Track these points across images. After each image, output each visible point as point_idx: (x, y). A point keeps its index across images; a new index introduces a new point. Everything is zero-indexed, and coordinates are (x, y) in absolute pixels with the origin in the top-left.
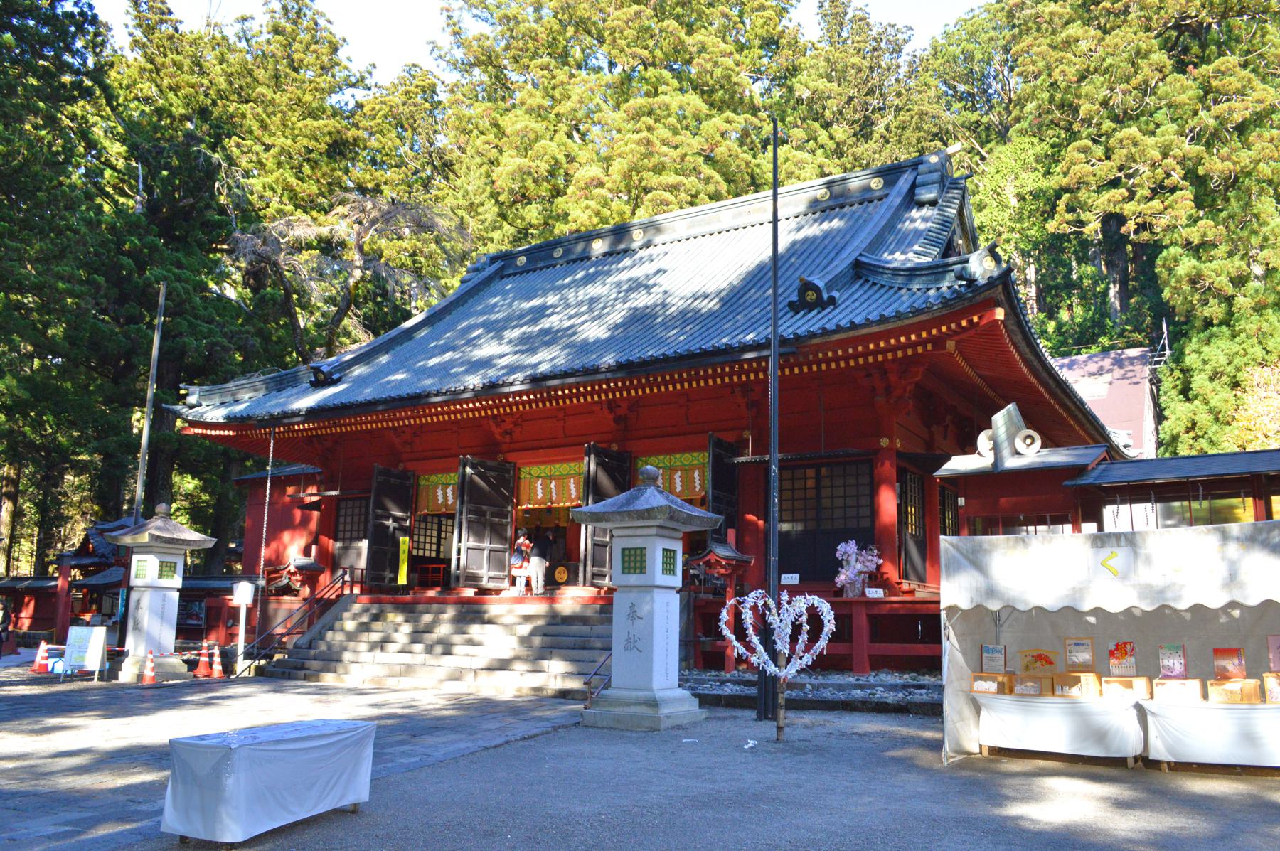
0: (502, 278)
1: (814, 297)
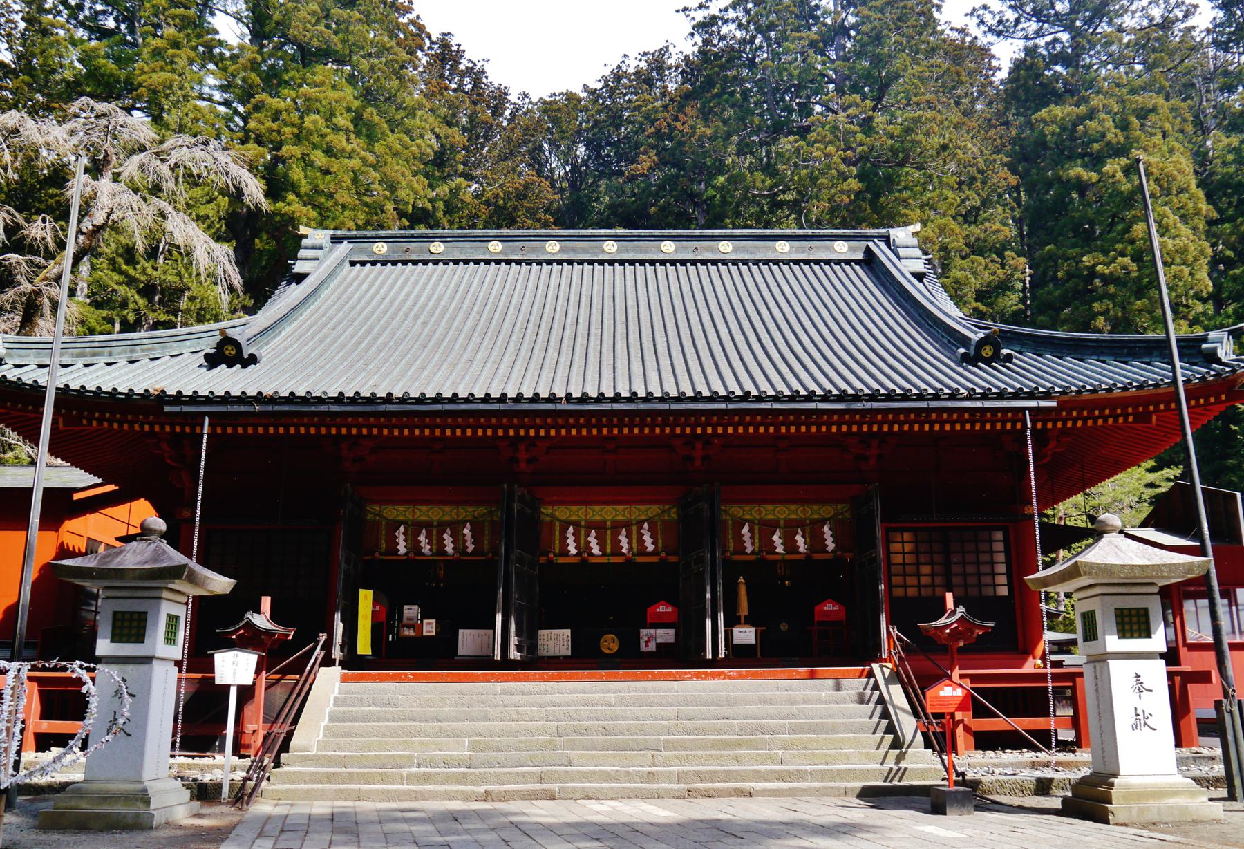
0: (353, 264)
1: (990, 353)
